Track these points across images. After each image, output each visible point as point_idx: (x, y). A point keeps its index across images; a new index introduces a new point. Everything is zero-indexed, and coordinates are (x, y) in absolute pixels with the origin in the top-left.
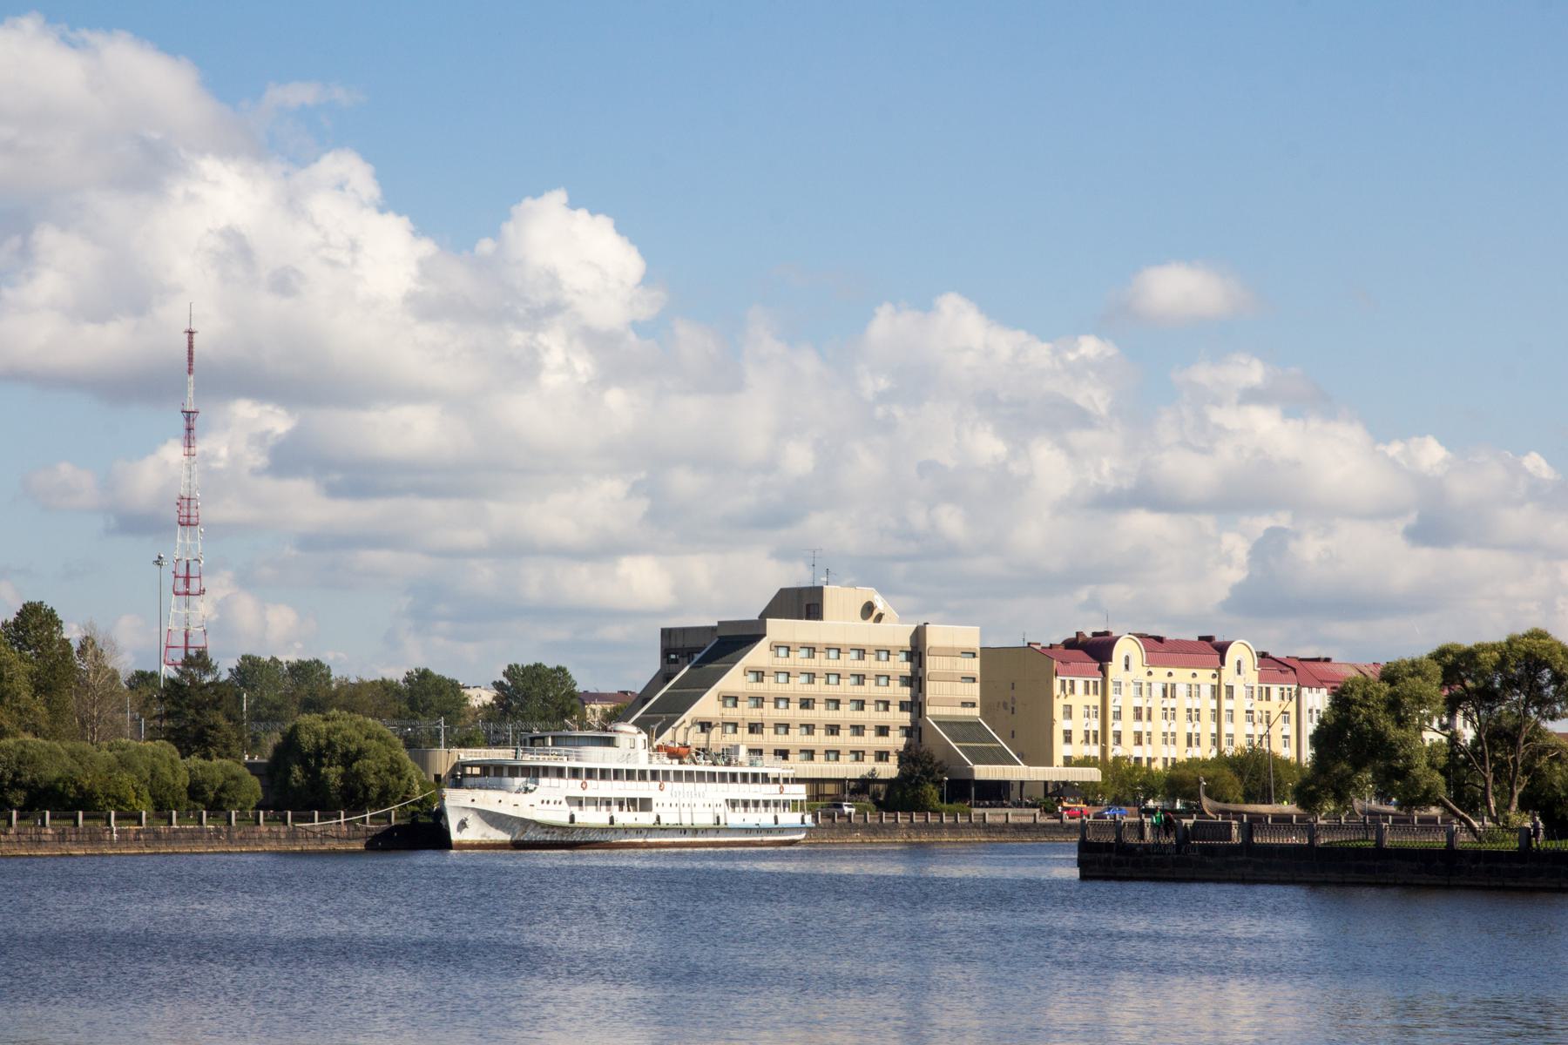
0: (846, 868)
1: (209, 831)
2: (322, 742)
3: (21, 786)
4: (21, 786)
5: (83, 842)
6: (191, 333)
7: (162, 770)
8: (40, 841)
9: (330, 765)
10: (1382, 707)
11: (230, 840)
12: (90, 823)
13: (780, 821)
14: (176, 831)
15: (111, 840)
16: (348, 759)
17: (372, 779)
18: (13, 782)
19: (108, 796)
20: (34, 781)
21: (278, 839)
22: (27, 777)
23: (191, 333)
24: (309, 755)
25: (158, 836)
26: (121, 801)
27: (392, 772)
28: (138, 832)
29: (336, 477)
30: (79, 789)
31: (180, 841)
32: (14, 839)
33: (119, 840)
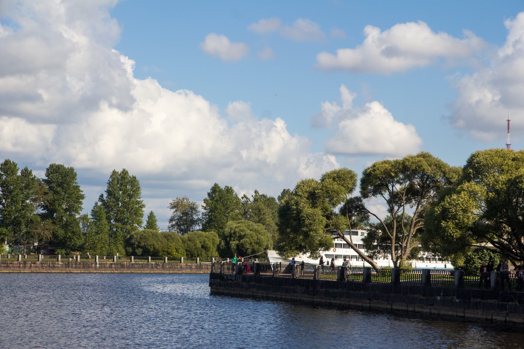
0: (169, 288)
1: (152, 265)
2: (232, 231)
3: (141, 247)
4: (141, 247)
5: (80, 268)
6: (509, 121)
7: (207, 242)
8: (54, 267)
9: (234, 240)
10: (306, 195)
11: (163, 267)
12: (83, 260)
13: (447, 267)
14: (132, 264)
15: (96, 267)
16: (241, 237)
17: (248, 246)
18: (137, 245)
19: (164, 251)
20: (145, 245)
21: (191, 268)
22: (143, 244)
23: (509, 121)
24: (227, 237)
25: (123, 266)
26: (169, 254)
27: (257, 243)
28: (111, 264)
29: (28, 107)
30: (154, 248)
31: (135, 268)
32: (40, 265)
33: (99, 267)
